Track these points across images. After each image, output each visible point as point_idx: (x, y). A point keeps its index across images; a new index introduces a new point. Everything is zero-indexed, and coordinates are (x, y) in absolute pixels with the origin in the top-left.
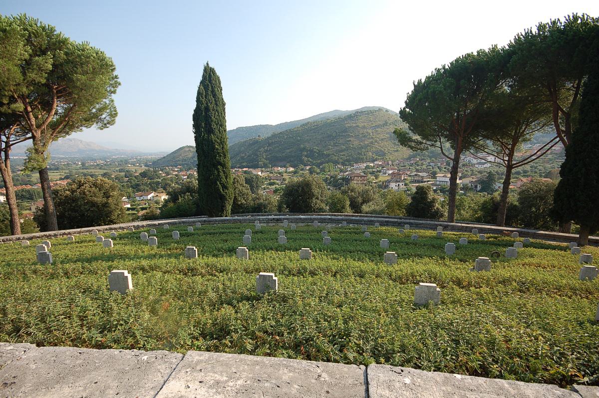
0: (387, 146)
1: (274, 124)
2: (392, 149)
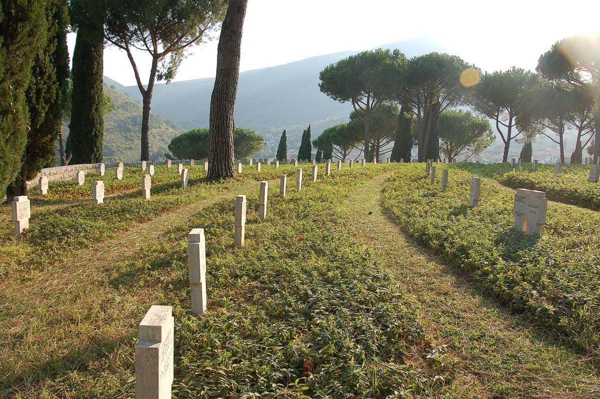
0: (116, 140)
1: (125, 85)
2: (123, 146)
